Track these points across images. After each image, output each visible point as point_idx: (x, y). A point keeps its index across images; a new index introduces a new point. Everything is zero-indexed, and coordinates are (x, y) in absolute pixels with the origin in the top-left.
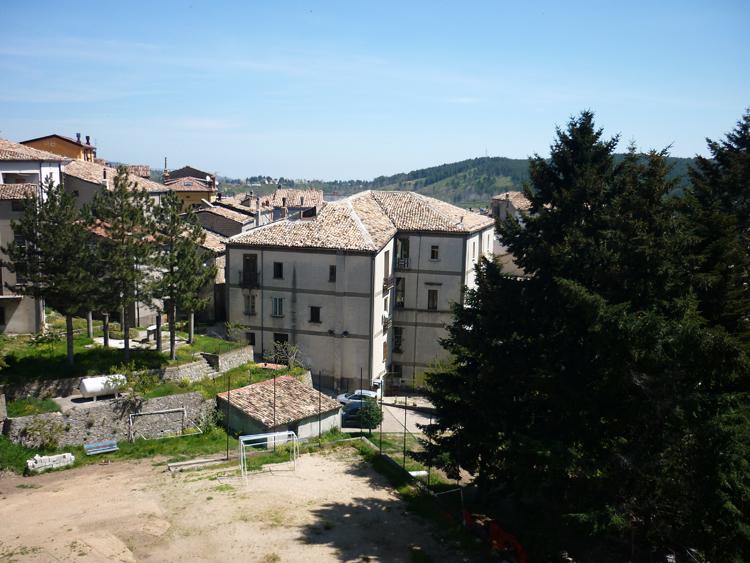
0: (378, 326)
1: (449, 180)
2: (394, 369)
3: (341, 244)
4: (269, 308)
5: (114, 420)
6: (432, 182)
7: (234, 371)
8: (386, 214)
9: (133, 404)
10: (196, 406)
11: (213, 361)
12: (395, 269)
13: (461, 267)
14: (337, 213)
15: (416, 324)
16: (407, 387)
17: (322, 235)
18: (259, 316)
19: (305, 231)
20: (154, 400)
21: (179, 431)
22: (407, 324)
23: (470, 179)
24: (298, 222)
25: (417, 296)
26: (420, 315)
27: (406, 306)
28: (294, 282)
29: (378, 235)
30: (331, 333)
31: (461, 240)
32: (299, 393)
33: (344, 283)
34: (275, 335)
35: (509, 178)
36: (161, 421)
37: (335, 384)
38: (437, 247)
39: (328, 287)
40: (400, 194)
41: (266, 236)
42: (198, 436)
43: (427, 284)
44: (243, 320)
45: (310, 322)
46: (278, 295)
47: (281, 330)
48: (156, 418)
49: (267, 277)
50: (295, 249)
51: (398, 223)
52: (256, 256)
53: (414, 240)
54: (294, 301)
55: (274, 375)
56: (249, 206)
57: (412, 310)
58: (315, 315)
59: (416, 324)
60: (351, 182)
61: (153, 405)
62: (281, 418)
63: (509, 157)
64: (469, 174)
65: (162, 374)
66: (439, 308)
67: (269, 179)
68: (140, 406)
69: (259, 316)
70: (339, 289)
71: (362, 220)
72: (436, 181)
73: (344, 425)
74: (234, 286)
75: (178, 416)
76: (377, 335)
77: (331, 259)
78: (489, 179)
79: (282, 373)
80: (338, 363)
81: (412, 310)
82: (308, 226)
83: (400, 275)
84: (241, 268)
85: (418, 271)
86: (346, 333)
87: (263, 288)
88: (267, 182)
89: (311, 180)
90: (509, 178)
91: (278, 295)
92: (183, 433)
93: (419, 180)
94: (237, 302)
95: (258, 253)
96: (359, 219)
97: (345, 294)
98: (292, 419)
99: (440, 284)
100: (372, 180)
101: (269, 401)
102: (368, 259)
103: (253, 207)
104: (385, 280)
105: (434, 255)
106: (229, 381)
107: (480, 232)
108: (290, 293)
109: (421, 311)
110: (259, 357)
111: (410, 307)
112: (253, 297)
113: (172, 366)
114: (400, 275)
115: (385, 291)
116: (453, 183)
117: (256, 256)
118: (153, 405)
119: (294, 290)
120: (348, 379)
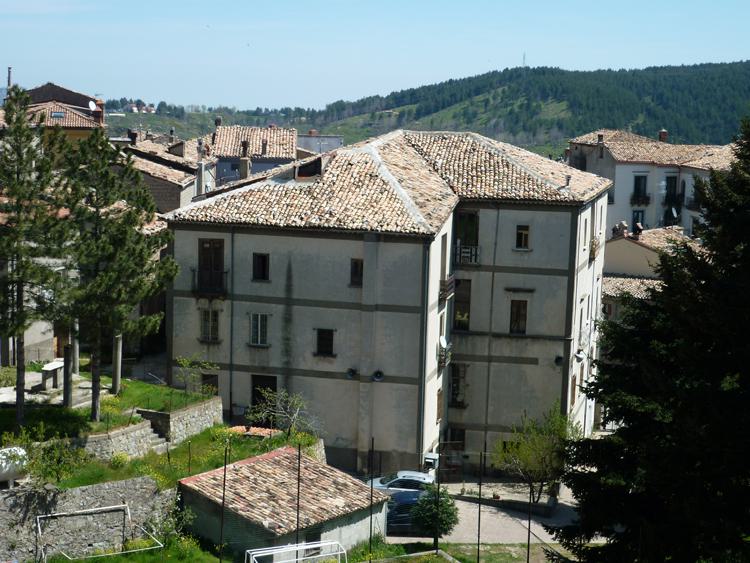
0: (432, 363)
1: (457, 108)
2: (452, 435)
3: (372, 222)
4: (244, 332)
5: (12, 526)
6: (428, 113)
7: (194, 439)
8: (437, 171)
9: (43, 499)
10: (146, 501)
11: (161, 428)
12: (455, 266)
13: (567, 263)
14: (355, 170)
15: (490, 359)
16: (473, 466)
17: (335, 206)
18: (226, 344)
19: (306, 200)
20: (77, 491)
21: (118, 545)
22: (474, 358)
23: (496, 108)
24: (291, 185)
25: (491, 310)
26: (496, 343)
27: (472, 327)
28: (289, 288)
29: (430, 208)
30: (353, 374)
31: (568, 215)
32: (313, 476)
33: (375, 289)
34: (253, 377)
35: (564, 105)
36: (88, 527)
37: (359, 461)
38: (526, 228)
39: (347, 294)
40: (455, 136)
41: (238, 208)
42: (151, 552)
43: (508, 290)
44: (199, 354)
45: (315, 355)
46: (261, 308)
47: (264, 369)
48: (80, 523)
49: (242, 279)
50: (290, 231)
51: (459, 186)
52: (221, 242)
53: (486, 217)
54: (288, 319)
55: (265, 446)
56: (182, 156)
57: (482, 334)
58: (325, 344)
59: (490, 359)
60: (286, 111)
61: (75, 500)
62: (288, 521)
63: (673, 65)
64: (494, 98)
65: (82, 444)
66: (530, 330)
67: (139, 104)
68: (54, 502)
69: (226, 344)
70: (367, 300)
71: (400, 181)
72: (437, 110)
73: (391, 532)
74: (182, 294)
75: (117, 518)
76: (432, 376)
77: (354, 249)
78: (528, 106)
79: (279, 442)
80: (364, 425)
81: (482, 334)
82: (309, 192)
83: (463, 275)
84: (194, 261)
85: (494, 269)
86: (379, 375)
87: (233, 297)
88: (135, 110)
89: (215, 106)
90: (564, 105)
91: (261, 308)
92: (125, 548)
93: (406, 108)
94: (188, 320)
95: (226, 237)
96: (395, 180)
97: (377, 308)
98: (313, 521)
99: (531, 291)
100: (323, 108)
101: (268, 491)
102: (419, 247)
103: (190, 156)
104: (442, 283)
105: (522, 239)
106: (195, 453)
107: (593, 202)
108: (281, 308)
109: (498, 336)
110: (230, 418)
111: (480, 330)
112: (216, 314)
113: (98, 431)
114: (463, 275)
115: (441, 301)
116: (465, 114)
117: (221, 242)
118: (75, 500)
119: (288, 302)
120: (381, 453)
